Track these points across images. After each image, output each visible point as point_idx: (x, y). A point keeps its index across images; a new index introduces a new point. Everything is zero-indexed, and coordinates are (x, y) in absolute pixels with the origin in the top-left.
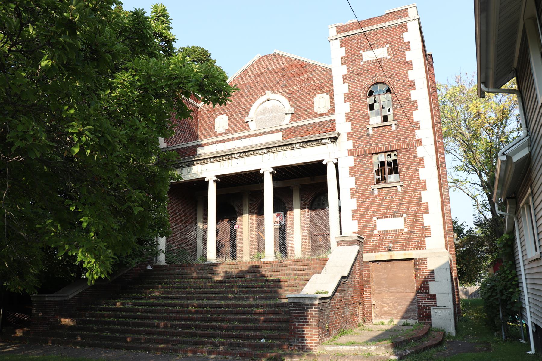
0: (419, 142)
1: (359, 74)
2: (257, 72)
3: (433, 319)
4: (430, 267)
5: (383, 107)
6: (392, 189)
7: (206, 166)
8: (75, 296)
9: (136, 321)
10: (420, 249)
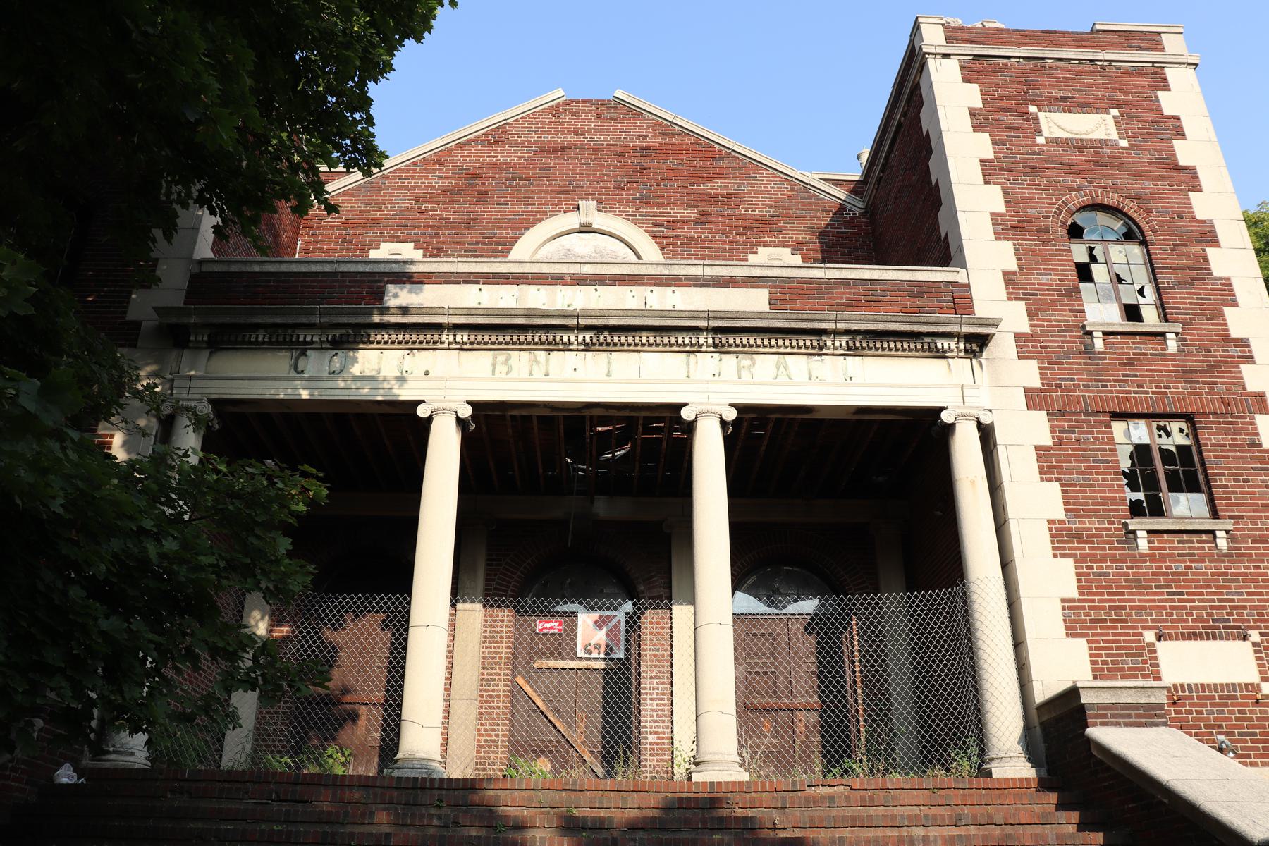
1: (1033, 168)
2: (546, 139)
5: (1120, 280)
6: (1195, 538)
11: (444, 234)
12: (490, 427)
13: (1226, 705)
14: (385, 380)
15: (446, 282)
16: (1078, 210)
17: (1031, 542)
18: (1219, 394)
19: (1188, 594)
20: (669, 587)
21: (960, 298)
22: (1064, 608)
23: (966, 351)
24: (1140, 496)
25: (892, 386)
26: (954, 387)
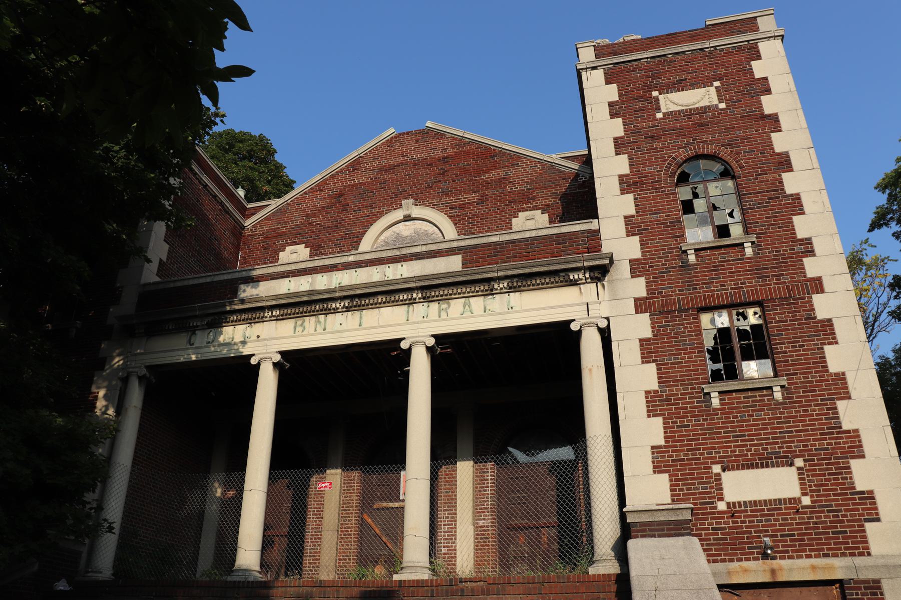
0: (817, 285)
1: (652, 137)
5: (715, 208)
7: (259, 329)
11: (323, 236)
12: (294, 365)
13: (773, 515)
14: (235, 344)
15: (272, 279)
16: (685, 162)
17: (632, 406)
18: (785, 283)
19: (749, 435)
20: (455, 450)
21: (593, 239)
22: (653, 453)
23: (591, 278)
24: (720, 366)
25: (538, 309)
26: (582, 304)
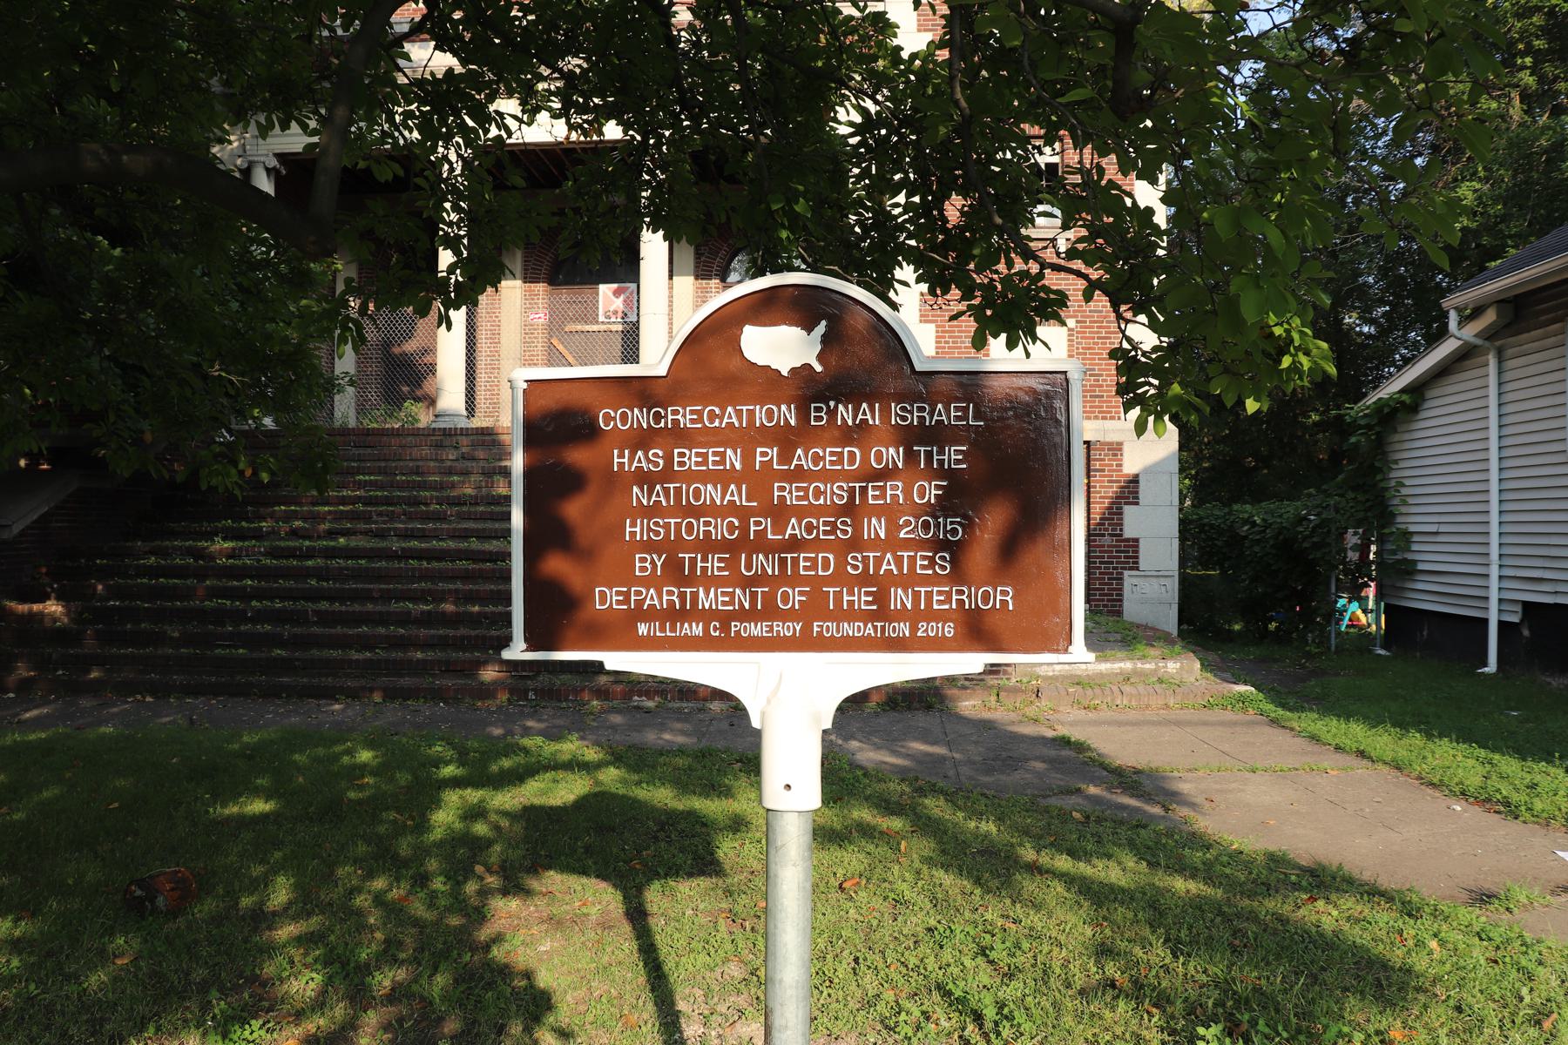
3: (1126, 604)
4: (1131, 466)
8: (28, 527)
9: (324, 605)
10: (1104, 418)
